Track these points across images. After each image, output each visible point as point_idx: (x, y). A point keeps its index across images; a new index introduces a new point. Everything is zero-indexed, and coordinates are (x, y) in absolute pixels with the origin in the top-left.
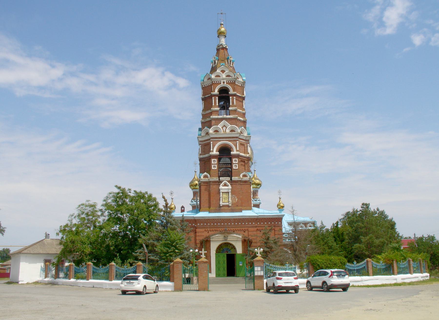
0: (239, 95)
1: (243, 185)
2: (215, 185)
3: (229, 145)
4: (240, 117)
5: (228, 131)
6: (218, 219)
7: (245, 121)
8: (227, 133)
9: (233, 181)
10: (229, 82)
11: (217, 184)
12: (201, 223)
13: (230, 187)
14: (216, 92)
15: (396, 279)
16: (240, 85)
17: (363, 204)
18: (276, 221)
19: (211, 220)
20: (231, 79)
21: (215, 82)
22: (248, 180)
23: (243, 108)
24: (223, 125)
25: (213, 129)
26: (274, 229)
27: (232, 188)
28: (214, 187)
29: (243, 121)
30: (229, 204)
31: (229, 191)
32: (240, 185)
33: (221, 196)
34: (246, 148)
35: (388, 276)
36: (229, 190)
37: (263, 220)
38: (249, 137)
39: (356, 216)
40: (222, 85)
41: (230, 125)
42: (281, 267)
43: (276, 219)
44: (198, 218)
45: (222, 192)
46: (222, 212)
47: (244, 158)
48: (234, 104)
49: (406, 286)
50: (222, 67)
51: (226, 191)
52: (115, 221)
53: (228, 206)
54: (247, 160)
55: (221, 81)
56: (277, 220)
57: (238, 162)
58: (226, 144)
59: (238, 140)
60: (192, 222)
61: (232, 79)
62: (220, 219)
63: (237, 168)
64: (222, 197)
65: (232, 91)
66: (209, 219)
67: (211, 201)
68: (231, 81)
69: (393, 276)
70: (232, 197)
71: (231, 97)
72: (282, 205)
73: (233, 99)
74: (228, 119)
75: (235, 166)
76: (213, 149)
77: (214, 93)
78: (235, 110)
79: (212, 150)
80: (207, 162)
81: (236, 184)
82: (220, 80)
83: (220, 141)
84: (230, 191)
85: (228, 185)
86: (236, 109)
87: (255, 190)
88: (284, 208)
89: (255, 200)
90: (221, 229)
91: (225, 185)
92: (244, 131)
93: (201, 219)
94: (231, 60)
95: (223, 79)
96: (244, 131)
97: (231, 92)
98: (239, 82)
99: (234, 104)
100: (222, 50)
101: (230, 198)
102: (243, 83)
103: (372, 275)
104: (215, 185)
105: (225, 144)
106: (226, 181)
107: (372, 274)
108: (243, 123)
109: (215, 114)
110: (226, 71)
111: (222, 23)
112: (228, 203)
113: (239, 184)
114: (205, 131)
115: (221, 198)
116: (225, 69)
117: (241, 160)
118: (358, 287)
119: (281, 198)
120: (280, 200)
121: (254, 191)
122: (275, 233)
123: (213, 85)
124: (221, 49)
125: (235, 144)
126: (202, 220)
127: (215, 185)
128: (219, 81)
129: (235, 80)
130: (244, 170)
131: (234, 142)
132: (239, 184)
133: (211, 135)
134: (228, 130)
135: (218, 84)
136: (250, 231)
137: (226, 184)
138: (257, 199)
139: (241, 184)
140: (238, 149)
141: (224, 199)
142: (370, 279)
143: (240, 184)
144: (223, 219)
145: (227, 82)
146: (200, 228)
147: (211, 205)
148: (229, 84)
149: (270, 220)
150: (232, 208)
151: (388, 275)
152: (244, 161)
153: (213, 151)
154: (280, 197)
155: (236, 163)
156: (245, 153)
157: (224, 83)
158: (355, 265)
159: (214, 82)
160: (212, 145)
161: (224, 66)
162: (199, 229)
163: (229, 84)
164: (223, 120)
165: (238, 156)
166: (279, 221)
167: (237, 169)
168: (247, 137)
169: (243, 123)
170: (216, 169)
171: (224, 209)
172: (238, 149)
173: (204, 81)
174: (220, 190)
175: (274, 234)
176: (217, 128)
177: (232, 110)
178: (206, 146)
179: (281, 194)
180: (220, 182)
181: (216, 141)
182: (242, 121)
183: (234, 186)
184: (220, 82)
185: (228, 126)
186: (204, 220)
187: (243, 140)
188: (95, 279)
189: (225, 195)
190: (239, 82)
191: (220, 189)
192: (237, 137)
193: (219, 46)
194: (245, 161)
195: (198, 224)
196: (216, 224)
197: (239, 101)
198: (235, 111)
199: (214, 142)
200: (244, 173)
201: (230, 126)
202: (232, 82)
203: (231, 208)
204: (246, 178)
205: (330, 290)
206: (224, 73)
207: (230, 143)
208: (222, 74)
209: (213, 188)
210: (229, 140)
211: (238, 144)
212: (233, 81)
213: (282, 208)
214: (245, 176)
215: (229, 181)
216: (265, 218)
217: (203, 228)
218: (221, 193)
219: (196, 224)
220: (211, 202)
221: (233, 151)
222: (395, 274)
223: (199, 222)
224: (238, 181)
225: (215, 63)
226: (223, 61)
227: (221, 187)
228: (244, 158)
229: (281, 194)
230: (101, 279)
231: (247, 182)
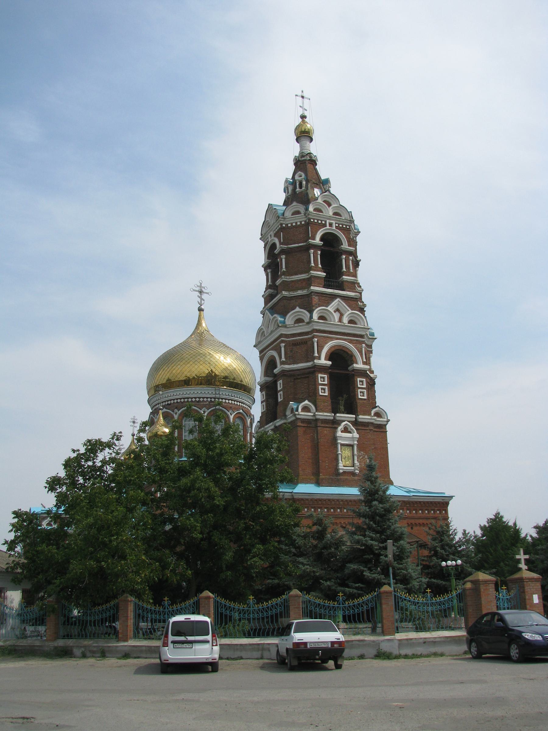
2: (327, 427)
3: (349, 350)
5: (345, 320)
6: (338, 500)
9: (361, 422)
10: (341, 226)
13: (356, 435)
14: (317, 240)
18: (438, 508)
19: (324, 502)
21: (314, 219)
24: (336, 308)
28: (325, 432)
31: (355, 443)
36: (353, 441)
39: (439, 527)
41: (349, 309)
44: (300, 497)
45: (342, 445)
52: (99, 501)
53: (353, 474)
55: (326, 222)
61: (346, 222)
62: (342, 501)
63: (365, 397)
65: (347, 245)
66: (320, 500)
70: (360, 456)
73: (347, 260)
75: (362, 394)
76: (319, 352)
77: (313, 241)
80: (299, 380)
83: (332, 339)
85: (352, 429)
90: (344, 521)
91: (346, 430)
93: (305, 499)
101: (356, 458)
109: (318, 284)
110: (332, 203)
112: (353, 468)
114: (294, 315)
116: (331, 200)
123: (311, 225)
126: (307, 499)
127: (327, 427)
133: (316, 324)
144: (346, 501)
145: (337, 225)
147: (321, 470)
153: (319, 358)
155: (325, 394)
158: (165, 609)
159: (312, 220)
160: (316, 344)
163: (340, 229)
164: (337, 298)
170: (326, 394)
171: (347, 479)
173: (285, 216)
178: (298, 347)
180: (335, 423)
186: (312, 500)
188: (90, 636)
189: (347, 453)
191: (339, 437)
193: (303, 156)
195: (332, 510)
196: (332, 510)
201: (350, 311)
202: (344, 226)
205: (483, 656)
207: (352, 347)
208: (328, 208)
209: (325, 432)
210: (348, 339)
212: (346, 226)
216: (420, 502)
218: (339, 446)
221: (357, 363)
225: (301, 187)
226: (317, 185)
227: (339, 434)
230: (90, 636)
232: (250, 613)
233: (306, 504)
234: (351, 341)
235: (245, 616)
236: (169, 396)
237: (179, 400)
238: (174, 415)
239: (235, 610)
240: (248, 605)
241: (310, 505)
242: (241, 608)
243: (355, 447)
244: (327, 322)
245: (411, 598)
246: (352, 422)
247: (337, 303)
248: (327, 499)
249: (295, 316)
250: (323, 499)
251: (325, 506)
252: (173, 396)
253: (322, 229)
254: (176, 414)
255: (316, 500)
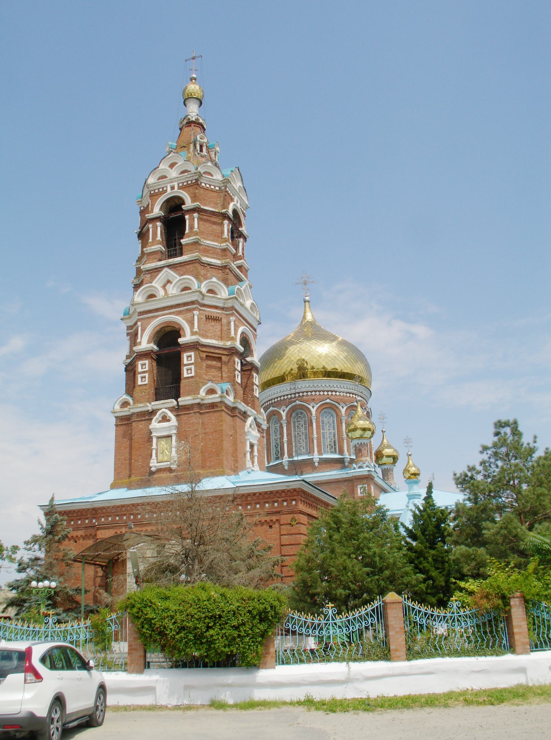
0: (211, 209)
1: (207, 415)
2: (142, 420)
4: (212, 258)
7: (225, 264)
8: (169, 296)
9: (182, 406)
10: (185, 184)
11: (147, 418)
12: (108, 516)
13: (174, 421)
15: (522, 670)
16: (217, 188)
17: (500, 425)
18: (283, 499)
20: (188, 178)
22: (219, 400)
23: (224, 238)
25: (144, 292)
26: (277, 520)
27: (178, 424)
28: (141, 426)
29: (220, 265)
30: (171, 464)
32: (198, 414)
33: (154, 446)
34: (225, 328)
35: (483, 659)
37: (249, 499)
38: (231, 300)
40: (169, 193)
42: (28, 627)
43: (283, 494)
45: (158, 438)
46: (154, 486)
47: (217, 351)
48: (195, 230)
49: (518, 705)
50: (170, 156)
51: (165, 434)
53: (170, 470)
54: (227, 355)
55: (167, 187)
56: (284, 497)
57: (195, 361)
58: (170, 321)
59: (194, 309)
60: (89, 515)
61: (191, 177)
63: (193, 374)
64: (157, 450)
66: (123, 506)
67: (133, 461)
68: (187, 182)
69: (509, 658)
71: (187, 217)
72: (413, 470)
74: (178, 264)
75: (189, 371)
77: (152, 214)
78: (194, 242)
79: (139, 340)
81: (188, 414)
82: (166, 185)
84: (175, 432)
86: (195, 240)
87: (358, 444)
88: (420, 478)
89: (359, 465)
91: (165, 419)
92: (219, 287)
94: (204, 142)
95: (172, 181)
96: (219, 287)
97: (189, 204)
98: (210, 181)
99: (194, 228)
100: (187, 128)
102: (223, 183)
103: (405, 657)
104: (143, 422)
105: (167, 322)
106: (166, 408)
107: (403, 652)
108: (221, 270)
111: (194, 76)
113: (195, 413)
115: (154, 452)
117: (207, 356)
118: (151, 713)
119: (410, 455)
120: (408, 458)
121: (357, 446)
122: (280, 532)
124: (186, 127)
125: (190, 319)
126: (109, 507)
127: (142, 420)
128: (163, 188)
129: (196, 177)
130: (219, 379)
131: (188, 314)
132: (195, 413)
134: (175, 289)
135: (157, 195)
136: (284, 535)
137: (166, 417)
138: (364, 463)
139: (201, 412)
140: (196, 329)
141: (162, 453)
142: (391, 673)
143: (199, 412)
145: (181, 185)
146: (105, 528)
148: (184, 188)
149: (267, 498)
150: (179, 473)
151: (485, 655)
152: (218, 357)
153: (140, 343)
154: (409, 453)
156: (221, 338)
157: (172, 188)
161: (174, 154)
162: (103, 531)
163: (184, 188)
165: (195, 346)
166: (292, 498)
167: (192, 377)
168: (229, 301)
169: (220, 271)
170: (146, 382)
172: (196, 329)
174: (151, 433)
175: (278, 534)
176: (151, 290)
177: (187, 244)
179: (411, 447)
181: (149, 318)
182: (219, 267)
183: (184, 418)
184: (165, 189)
185: (175, 280)
187: (216, 307)
190: (210, 181)
191: (152, 429)
192: (193, 303)
194: (221, 358)
195: (103, 520)
197: (211, 223)
198: (196, 243)
199: (145, 322)
200: (208, 385)
201: (179, 278)
203: (175, 474)
204: (213, 396)
206: (174, 168)
211: (196, 318)
212: (192, 181)
213: (413, 476)
214: (211, 391)
215: (172, 409)
217: (112, 528)
218: (154, 440)
219: (98, 519)
220: (133, 464)
222: (518, 648)
223: (104, 513)
224: (192, 405)
228: (217, 351)
229: (411, 447)
231: (217, 406)
232: (322, 629)
233: (109, 513)
234: (179, 313)
235: (308, 631)
236: (270, 394)
237: (301, 393)
238: (340, 407)
239: (446, 619)
240: (325, 616)
241: (113, 513)
242: (316, 622)
243: (174, 438)
244: (157, 298)
245: (314, 618)
246: (169, 408)
247: (165, 275)
248: (131, 504)
249: (147, 292)
250: (126, 505)
251: (130, 512)
252: (280, 393)
253: (160, 198)
254: (313, 407)
255: (118, 507)
